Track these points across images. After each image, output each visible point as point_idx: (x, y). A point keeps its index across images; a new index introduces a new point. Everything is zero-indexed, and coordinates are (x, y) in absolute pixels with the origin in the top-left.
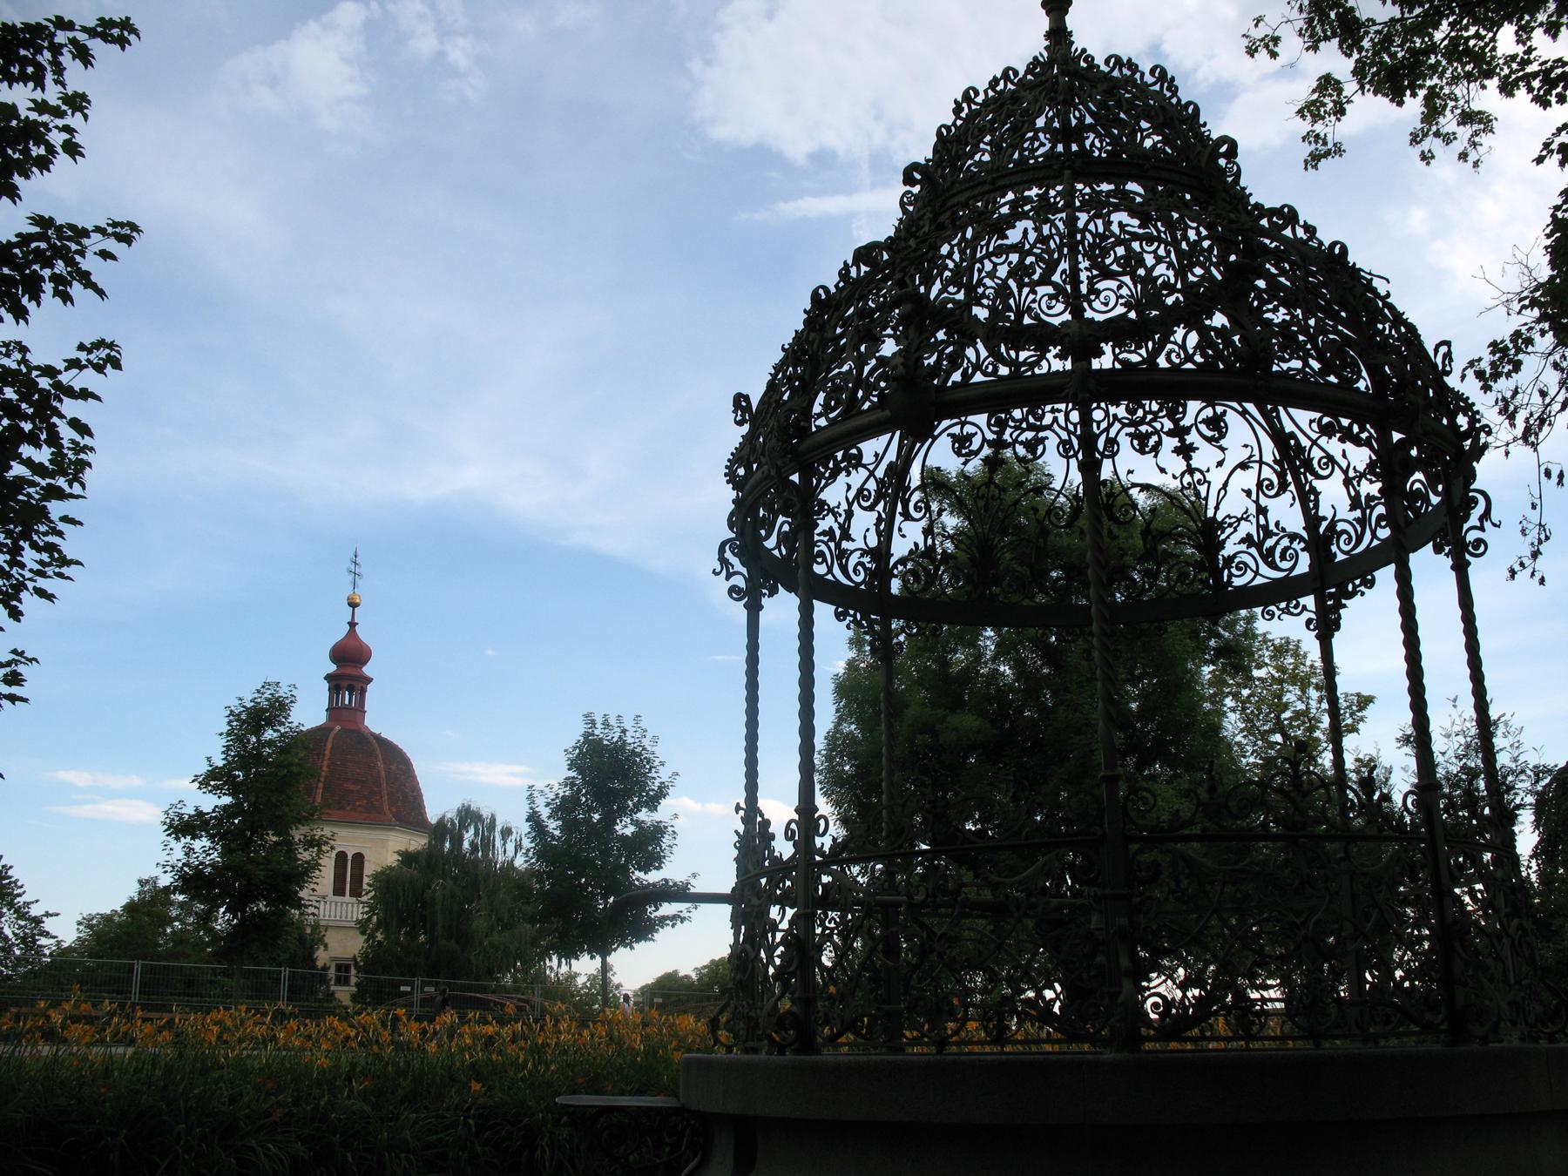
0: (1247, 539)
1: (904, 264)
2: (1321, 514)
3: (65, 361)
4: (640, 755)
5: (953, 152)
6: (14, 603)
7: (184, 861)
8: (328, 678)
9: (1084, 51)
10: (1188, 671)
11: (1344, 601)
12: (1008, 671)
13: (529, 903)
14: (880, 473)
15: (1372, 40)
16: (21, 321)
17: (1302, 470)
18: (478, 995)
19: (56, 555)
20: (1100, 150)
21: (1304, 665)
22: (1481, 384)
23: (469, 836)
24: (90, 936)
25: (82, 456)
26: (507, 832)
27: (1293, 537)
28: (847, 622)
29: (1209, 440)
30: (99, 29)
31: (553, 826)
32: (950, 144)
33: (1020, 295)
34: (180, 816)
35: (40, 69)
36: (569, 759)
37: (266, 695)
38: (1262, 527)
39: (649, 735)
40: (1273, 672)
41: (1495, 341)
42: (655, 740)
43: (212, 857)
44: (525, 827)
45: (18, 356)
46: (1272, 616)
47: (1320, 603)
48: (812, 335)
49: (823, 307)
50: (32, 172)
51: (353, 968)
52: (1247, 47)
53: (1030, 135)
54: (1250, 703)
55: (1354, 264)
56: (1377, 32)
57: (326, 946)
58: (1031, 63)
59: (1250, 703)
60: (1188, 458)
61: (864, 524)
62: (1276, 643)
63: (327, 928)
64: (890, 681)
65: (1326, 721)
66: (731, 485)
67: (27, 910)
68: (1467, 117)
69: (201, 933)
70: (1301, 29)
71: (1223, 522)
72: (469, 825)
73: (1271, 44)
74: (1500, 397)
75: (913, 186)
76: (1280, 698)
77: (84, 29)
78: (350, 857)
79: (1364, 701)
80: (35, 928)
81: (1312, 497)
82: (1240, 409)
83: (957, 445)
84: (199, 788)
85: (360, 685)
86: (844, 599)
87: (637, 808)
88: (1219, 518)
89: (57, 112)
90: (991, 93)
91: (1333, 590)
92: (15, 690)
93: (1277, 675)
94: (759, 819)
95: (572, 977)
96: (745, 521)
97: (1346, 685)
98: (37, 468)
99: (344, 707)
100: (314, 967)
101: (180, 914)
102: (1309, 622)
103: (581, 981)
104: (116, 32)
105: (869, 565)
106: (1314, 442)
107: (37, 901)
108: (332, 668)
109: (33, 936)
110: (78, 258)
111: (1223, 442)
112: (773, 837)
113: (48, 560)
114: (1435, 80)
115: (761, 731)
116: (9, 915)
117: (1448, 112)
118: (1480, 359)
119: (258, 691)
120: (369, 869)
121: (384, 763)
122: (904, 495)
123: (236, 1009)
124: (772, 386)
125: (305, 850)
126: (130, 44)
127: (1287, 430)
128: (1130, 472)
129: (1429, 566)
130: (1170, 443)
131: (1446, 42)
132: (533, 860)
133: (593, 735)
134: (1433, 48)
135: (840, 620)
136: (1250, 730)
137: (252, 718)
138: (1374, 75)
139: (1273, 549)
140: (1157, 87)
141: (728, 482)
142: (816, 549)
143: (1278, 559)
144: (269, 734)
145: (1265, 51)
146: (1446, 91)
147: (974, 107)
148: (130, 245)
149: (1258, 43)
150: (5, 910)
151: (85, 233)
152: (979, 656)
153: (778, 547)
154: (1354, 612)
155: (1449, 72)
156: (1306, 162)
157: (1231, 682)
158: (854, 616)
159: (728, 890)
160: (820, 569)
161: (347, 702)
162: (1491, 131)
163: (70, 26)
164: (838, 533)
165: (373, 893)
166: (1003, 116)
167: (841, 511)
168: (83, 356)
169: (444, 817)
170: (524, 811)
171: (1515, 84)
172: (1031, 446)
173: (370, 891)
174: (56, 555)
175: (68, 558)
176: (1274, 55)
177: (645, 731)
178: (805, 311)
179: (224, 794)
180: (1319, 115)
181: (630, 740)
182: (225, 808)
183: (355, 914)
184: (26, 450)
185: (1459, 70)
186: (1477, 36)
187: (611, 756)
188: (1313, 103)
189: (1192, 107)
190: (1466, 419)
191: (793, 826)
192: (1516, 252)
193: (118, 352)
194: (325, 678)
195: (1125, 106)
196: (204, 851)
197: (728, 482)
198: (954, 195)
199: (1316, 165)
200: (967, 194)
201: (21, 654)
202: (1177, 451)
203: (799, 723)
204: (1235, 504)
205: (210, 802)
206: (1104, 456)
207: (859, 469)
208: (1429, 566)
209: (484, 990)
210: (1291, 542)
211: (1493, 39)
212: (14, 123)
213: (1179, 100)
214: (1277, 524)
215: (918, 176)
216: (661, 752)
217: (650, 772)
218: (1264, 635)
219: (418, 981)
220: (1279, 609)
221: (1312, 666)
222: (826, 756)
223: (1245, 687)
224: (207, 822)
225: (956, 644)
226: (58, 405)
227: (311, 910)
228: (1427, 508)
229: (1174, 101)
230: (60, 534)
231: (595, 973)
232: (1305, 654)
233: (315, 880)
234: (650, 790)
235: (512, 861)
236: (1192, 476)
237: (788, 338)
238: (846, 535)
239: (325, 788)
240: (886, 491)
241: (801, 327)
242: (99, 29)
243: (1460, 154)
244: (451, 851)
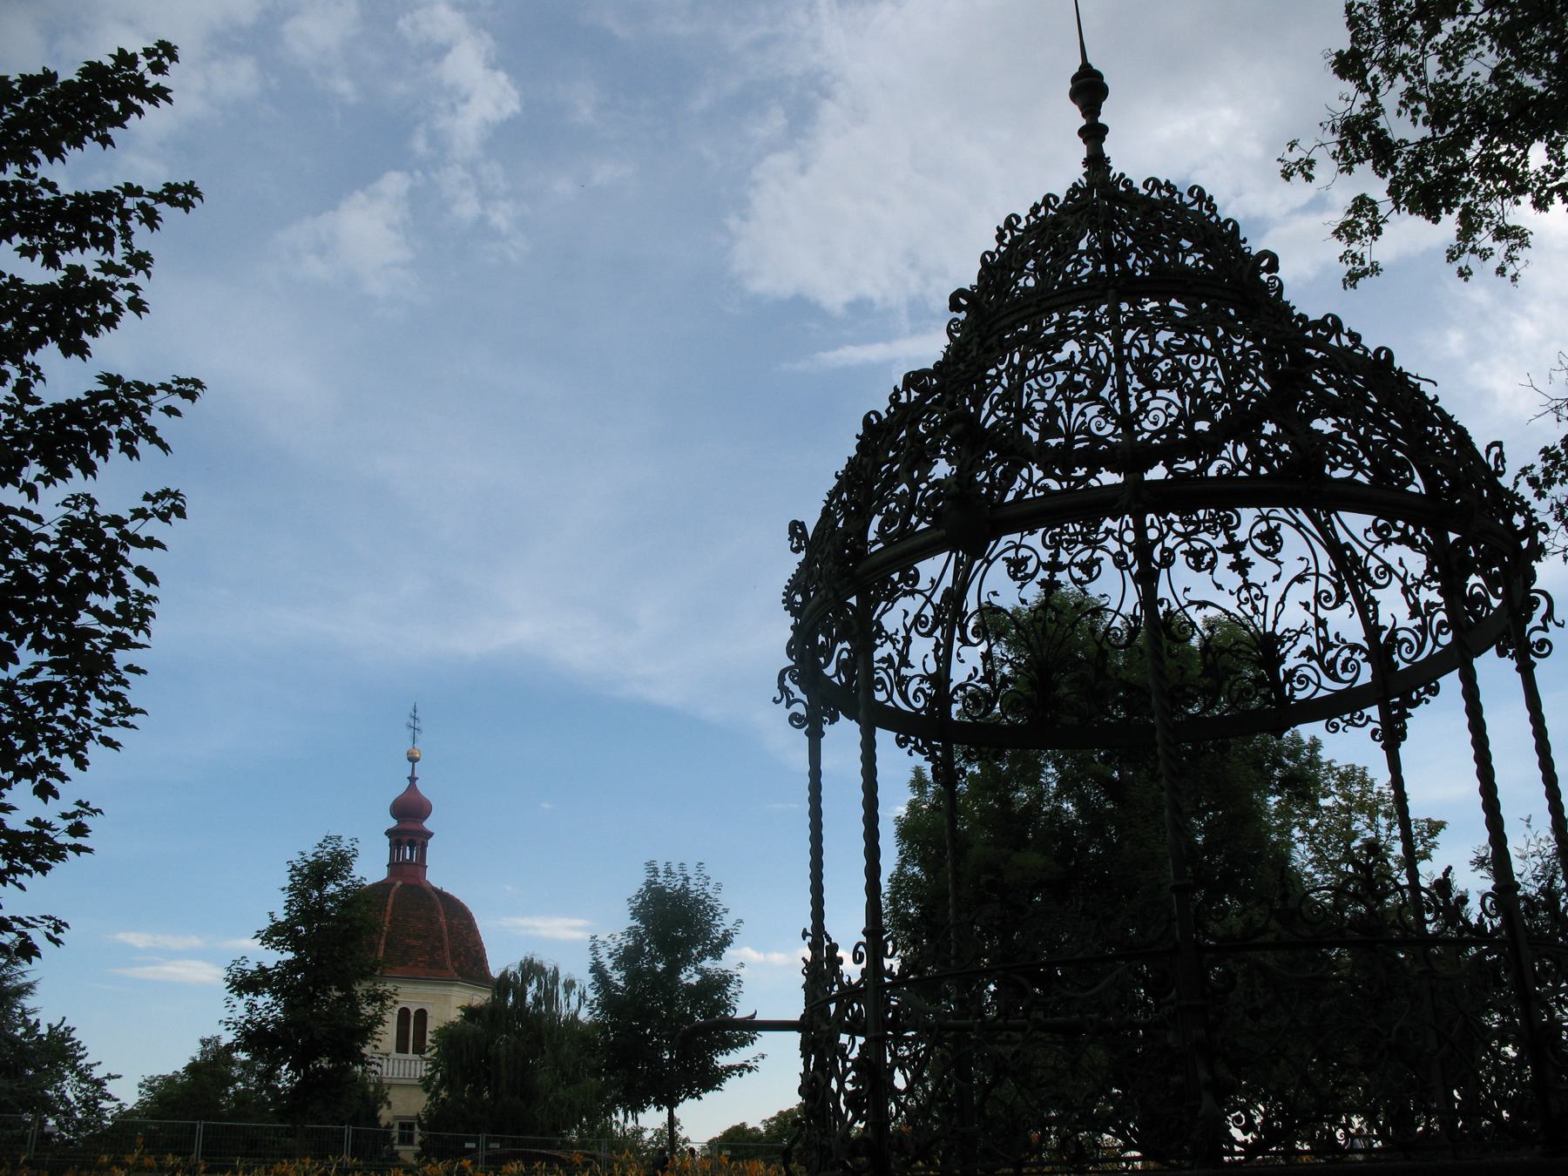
0: (1308, 653)
1: (954, 386)
2: (1380, 623)
3: (131, 511)
4: (703, 902)
5: (998, 278)
6: (80, 752)
7: (247, 1018)
8: (389, 833)
9: (1122, 175)
10: (1253, 802)
11: (1409, 710)
12: (1071, 808)
13: (593, 1056)
14: (936, 599)
15: (1405, 160)
16: (89, 476)
17: (1360, 581)
18: (544, 1151)
19: (121, 705)
20: (1143, 269)
21: (1372, 792)
22: (1535, 491)
23: (532, 990)
24: (152, 1098)
25: (146, 606)
26: (570, 985)
27: (1354, 648)
28: (908, 748)
29: (1264, 554)
30: (165, 194)
31: (617, 977)
32: (995, 270)
33: (1069, 418)
34: (243, 972)
35: (110, 234)
36: (632, 908)
37: (327, 849)
38: (1322, 639)
39: (712, 882)
40: (1340, 801)
41: (1546, 448)
42: (718, 887)
43: (275, 1013)
44: (589, 978)
45: (85, 508)
46: (1337, 728)
47: (1384, 713)
48: (865, 460)
49: (875, 434)
50: (100, 330)
51: (416, 1126)
52: (1282, 171)
53: (1074, 257)
54: (1318, 832)
55: (1401, 368)
56: (1410, 152)
57: (389, 1104)
58: (1070, 189)
59: (1318, 832)
60: (1244, 574)
61: (922, 650)
62: (1341, 770)
63: (390, 1086)
64: (953, 822)
65: (1398, 849)
66: (789, 612)
67: (89, 1072)
68: (1502, 233)
69: (264, 1093)
70: (1335, 152)
71: (1282, 636)
72: (532, 978)
73: (1306, 168)
74: (1555, 503)
75: (960, 312)
76: (1348, 826)
77: (151, 195)
78: (412, 1014)
79: (1435, 827)
80: (97, 1090)
81: (1371, 607)
82: (1294, 523)
83: (1012, 569)
84: (262, 944)
85: (422, 839)
86: (907, 727)
87: (701, 956)
88: (1278, 632)
89: (123, 272)
90: (1032, 219)
91: (1397, 700)
92: (80, 840)
93: (1344, 803)
94: (826, 943)
95: (639, 1132)
96: (804, 650)
97: (1416, 811)
98: (104, 617)
99: (405, 862)
100: (380, 1126)
101: (242, 1074)
102: (1374, 732)
103: (647, 1135)
104: (180, 196)
105: (929, 691)
106: (1370, 552)
107: (99, 1063)
108: (393, 823)
109: (95, 1099)
110: (144, 415)
111: (1278, 556)
112: (840, 961)
113: (112, 709)
114: (1469, 198)
115: (826, 845)
116: (71, 1077)
117: (1483, 229)
118: (1532, 467)
119: (320, 845)
120: (432, 1025)
121: (447, 918)
122: (961, 620)
123: (300, 1162)
124: (826, 513)
125: (368, 1005)
126: (194, 207)
127: (1343, 541)
128: (1187, 590)
129: (1493, 669)
130: (1226, 559)
131: (1477, 161)
132: (598, 1012)
133: (656, 883)
134: (1465, 167)
135: (902, 747)
136: (1319, 862)
137: (313, 873)
138: (1409, 194)
139: (1334, 660)
140: (1196, 207)
141: (786, 609)
142: (876, 676)
143: (1339, 671)
144: (331, 888)
145: (1300, 174)
146: (1481, 208)
147: (1016, 233)
148: (193, 401)
149: (1293, 167)
150: (67, 1073)
151: (151, 390)
152: (1041, 795)
153: (837, 674)
154: (1420, 721)
155: (1482, 189)
156: (1344, 281)
157: (1298, 812)
158: (916, 742)
159: (797, 1018)
160: (880, 696)
161: (408, 857)
162: (1527, 245)
163: (138, 192)
164: (896, 660)
165: (436, 1049)
166: (1045, 241)
167: (899, 637)
168: (148, 506)
169: (506, 971)
170: (587, 961)
171: (1549, 197)
172: (1087, 567)
173: (433, 1048)
174: (121, 705)
175: (132, 707)
176: (1309, 178)
177: (709, 878)
178: (858, 436)
179: (287, 950)
180: (1356, 236)
181: (693, 888)
182: (288, 963)
183: (418, 1070)
184: (94, 599)
185: (1492, 187)
186: (1510, 153)
187: (674, 905)
188: (1348, 223)
189: (1231, 224)
190: (1523, 518)
191: (861, 949)
192: (1563, 359)
193: (182, 501)
194: (386, 834)
195: (1166, 226)
196: (267, 1008)
197: (786, 609)
198: (1000, 319)
199: (1354, 284)
200: (1013, 318)
201: (86, 805)
202: (1232, 567)
203: (865, 880)
204: (1294, 617)
205: (273, 958)
206: (1161, 566)
207: (916, 595)
208: (1493, 669)
209: (550, 1145)
210: (1352, 653)
211: (1525, 155)
212: (83, 284)
213: (1218, 219)
214: (1337, 635)
215: (964, 302)
216: (724, 899)
217: (714, 920)
218: (1329, 763)
219: (482, 1137)
220: (1343, 721)
221: (1379, 793)
222: (890, 899)
223: (1312, 817)
224: (269, 978)
225: (1018, 782)
226: (124, 553)
227: (374, 1067)
228: (1488, 611)
229: (1213, 219)
230: (125, 683)
231: (662, 1128)
232: (1372, 780)
233: (377, 1036)
234: (714, 938)
235: (576, 1013)
236: (1249, 592)
237: (841, 466)
238: (905, 662)
239: (387, 944)
240: (944, 616)
241: (853, 453)
242: (165, 194)
243: (1498, 269)
244: (515, 1004)
